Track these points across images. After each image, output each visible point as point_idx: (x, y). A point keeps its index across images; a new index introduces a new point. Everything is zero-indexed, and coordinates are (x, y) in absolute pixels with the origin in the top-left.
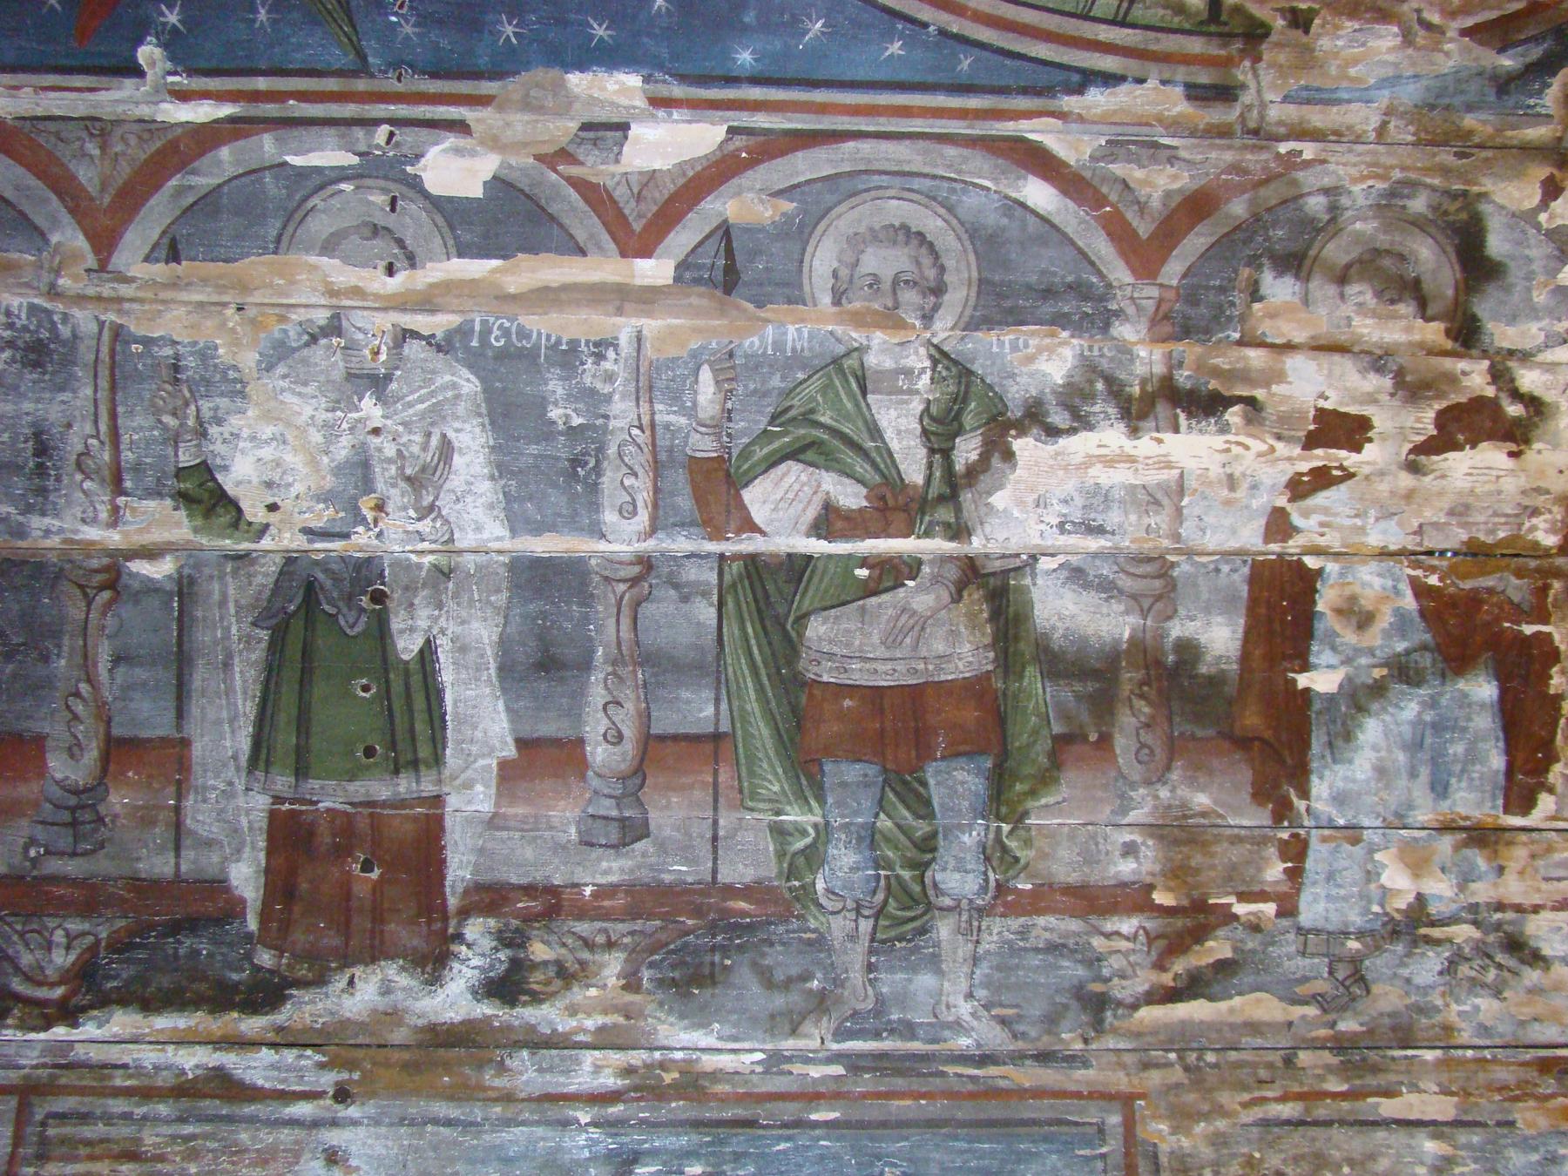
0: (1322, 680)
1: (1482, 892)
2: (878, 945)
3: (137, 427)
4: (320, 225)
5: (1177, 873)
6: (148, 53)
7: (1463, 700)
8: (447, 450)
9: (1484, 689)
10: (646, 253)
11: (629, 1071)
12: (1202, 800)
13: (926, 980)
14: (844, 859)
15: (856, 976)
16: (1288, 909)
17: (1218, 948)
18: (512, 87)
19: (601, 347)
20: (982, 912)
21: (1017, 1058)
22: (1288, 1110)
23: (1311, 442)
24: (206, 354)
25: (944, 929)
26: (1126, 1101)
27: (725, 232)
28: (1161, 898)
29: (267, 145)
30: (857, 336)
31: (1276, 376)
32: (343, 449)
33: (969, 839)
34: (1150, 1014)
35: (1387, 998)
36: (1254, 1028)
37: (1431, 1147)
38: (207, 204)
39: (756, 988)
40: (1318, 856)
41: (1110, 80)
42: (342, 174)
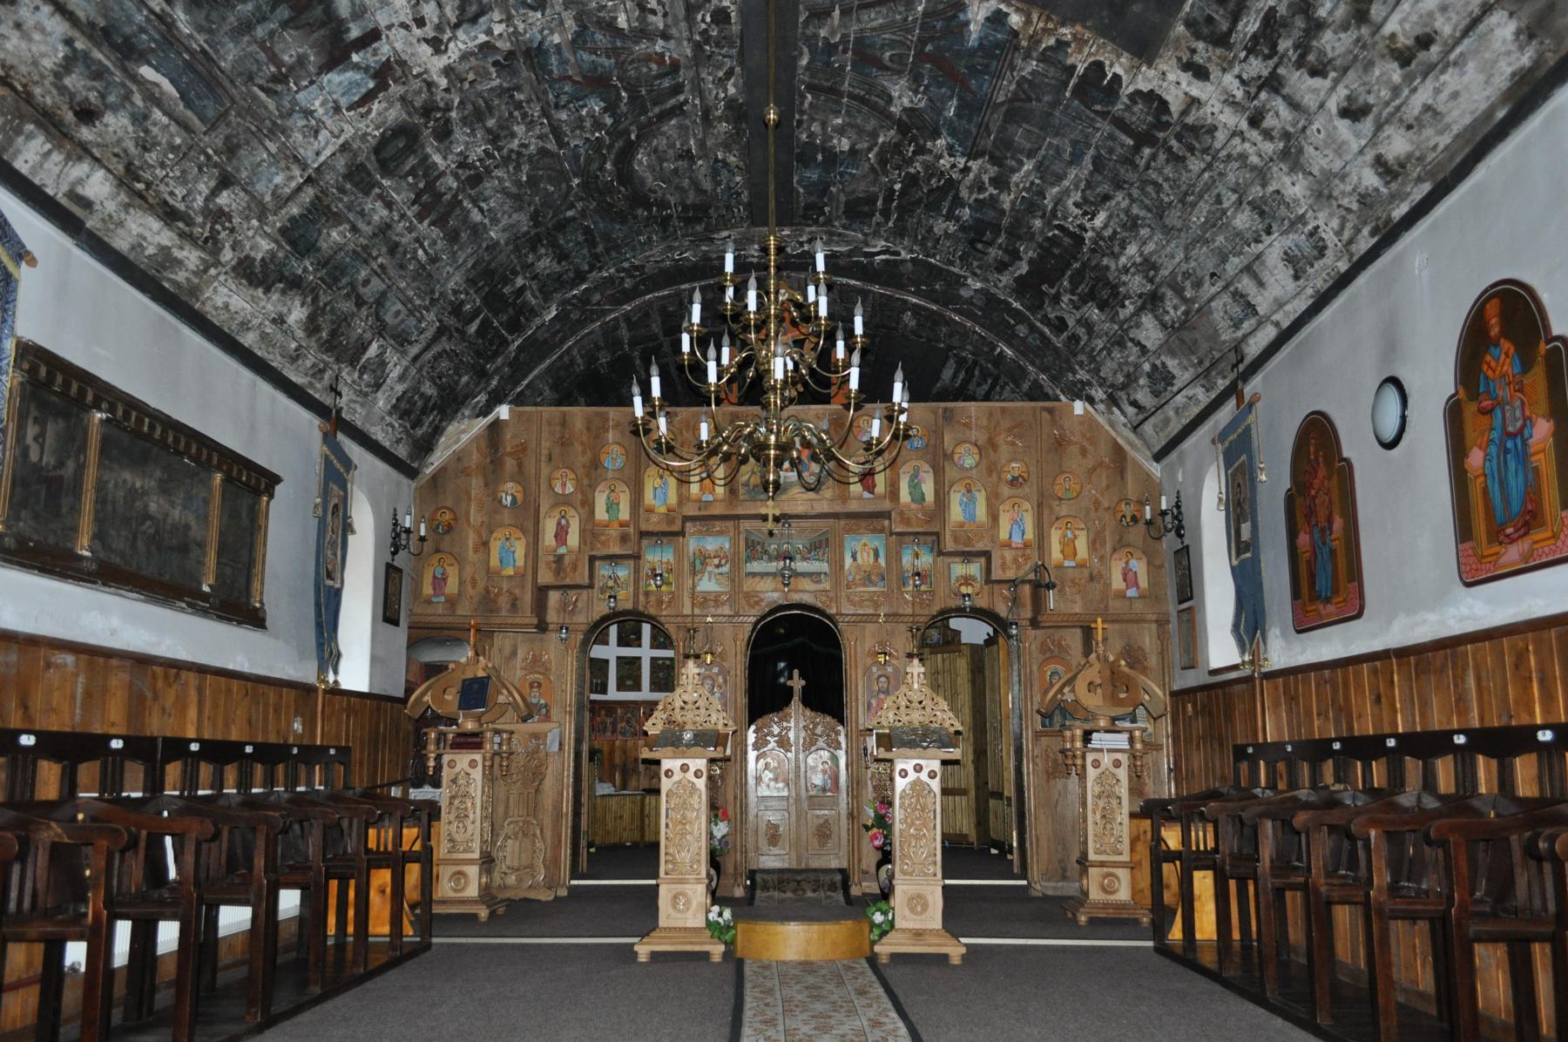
0: (355, 58)
1: (324, 118)
2: (233, 30)
5: (291, 68)
7: (366, 84)
9: (371, 85)
11: (163, 10)
12: (312, 58)
13: (231, 45)
15: (222, 32)
16: (296, 92)
17: (279, 88)
20: (256, 42)
21: (228, 77)
22: (253, 128)
23: (415, 20)
25: (246, 39)
26: (233, 101)
28: (284, 70)
30: (490, 418)
33: (272, 26)
34: (255, 89)
35: (289, 123)
36: (266, 108)
37: (265, 156)
39: (203, 16)
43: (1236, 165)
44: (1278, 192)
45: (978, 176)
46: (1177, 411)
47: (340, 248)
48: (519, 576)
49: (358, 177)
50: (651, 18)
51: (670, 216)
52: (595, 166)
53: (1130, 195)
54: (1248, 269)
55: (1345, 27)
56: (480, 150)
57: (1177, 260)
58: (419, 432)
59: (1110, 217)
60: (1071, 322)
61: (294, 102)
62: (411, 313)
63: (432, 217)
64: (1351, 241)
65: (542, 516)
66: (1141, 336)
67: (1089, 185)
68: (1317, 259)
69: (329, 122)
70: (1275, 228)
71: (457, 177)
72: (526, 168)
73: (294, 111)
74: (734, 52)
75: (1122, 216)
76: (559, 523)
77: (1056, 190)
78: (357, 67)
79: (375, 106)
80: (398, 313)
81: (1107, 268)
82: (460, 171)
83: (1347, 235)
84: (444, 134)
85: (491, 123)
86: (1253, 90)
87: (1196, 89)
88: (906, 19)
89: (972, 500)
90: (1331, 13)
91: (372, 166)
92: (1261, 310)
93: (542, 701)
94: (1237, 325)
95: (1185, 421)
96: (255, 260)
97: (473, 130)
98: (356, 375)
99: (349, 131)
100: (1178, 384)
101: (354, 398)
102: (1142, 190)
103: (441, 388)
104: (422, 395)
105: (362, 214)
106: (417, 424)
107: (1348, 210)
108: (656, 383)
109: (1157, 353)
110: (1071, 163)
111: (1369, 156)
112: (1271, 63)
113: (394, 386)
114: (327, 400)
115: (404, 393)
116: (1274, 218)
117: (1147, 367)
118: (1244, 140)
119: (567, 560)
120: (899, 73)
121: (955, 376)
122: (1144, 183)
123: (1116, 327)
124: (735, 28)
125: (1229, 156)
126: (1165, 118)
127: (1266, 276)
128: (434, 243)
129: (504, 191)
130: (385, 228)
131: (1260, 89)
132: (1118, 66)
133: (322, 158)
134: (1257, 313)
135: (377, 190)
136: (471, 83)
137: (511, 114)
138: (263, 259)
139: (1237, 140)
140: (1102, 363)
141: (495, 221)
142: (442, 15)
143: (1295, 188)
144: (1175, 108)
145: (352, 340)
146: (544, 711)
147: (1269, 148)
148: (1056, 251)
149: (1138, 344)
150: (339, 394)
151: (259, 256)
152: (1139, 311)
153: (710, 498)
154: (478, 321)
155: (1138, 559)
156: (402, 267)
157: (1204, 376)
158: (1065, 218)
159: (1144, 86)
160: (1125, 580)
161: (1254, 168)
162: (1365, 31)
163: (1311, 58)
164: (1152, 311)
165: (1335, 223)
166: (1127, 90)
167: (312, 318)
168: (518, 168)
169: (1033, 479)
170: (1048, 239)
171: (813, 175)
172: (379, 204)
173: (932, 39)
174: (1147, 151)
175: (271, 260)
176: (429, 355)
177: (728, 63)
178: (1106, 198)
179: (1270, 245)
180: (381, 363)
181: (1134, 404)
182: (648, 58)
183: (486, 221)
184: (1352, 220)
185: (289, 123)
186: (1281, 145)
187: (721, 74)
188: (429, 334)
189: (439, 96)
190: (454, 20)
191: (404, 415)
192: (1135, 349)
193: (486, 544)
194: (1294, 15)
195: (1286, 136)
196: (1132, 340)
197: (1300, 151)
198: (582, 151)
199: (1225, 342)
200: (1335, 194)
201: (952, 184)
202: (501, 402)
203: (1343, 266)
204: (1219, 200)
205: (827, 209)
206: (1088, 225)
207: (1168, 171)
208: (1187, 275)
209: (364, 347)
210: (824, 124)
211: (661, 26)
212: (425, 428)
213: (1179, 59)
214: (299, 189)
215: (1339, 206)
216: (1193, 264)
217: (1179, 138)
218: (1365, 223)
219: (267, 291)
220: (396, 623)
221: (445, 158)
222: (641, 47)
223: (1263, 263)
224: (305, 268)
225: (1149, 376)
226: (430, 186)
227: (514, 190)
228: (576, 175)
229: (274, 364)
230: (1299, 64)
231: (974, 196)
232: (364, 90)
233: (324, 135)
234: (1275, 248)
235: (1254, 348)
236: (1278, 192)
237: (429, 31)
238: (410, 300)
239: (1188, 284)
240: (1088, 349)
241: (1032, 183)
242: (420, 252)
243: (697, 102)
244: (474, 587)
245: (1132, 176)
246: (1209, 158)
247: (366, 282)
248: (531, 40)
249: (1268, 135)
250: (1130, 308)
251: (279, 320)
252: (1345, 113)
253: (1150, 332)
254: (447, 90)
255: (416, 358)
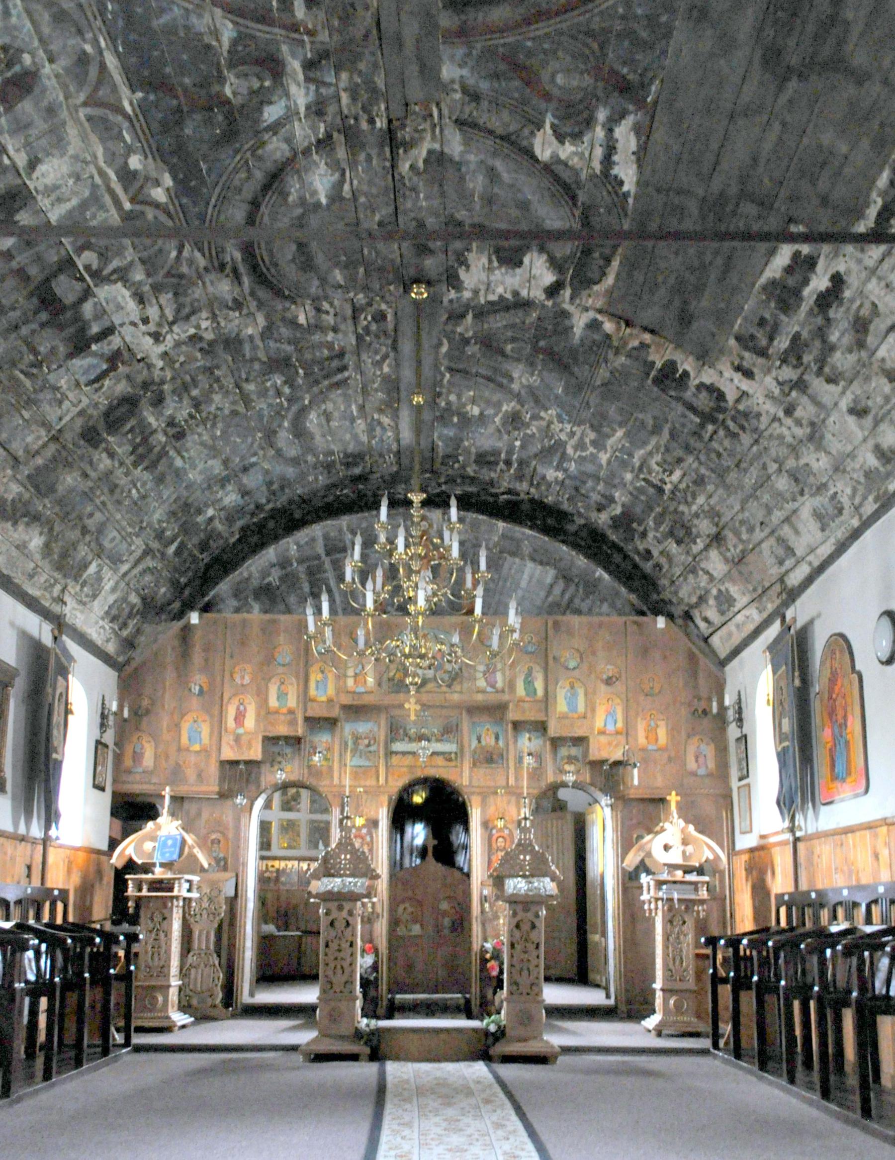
0: (94, 347)
3: (43, 142)
4: (110, 144)
6: (140, 95)
8: (69, 200)
9: (105, 367)
10: (131, 203)
14: (18, 313)
17: (35, 371)
18: (161, 164)
19: (108, 211)
24: (69, 143)
27: (143, 213)
29: (126, 125)
31: (151, 306)
32: (58, 183)
34: (17, 373)
37: (21, 422)
38: (104, 120)
40: (63, 369)
41: (204, 255)
42: (125, 142)
43: (776, 442)
44: (807, 465)
45: (582, 438)
46: (737, 626)
47: (71, 490)
48: (205, 751)
49: (91, 436)
50: (324, 316)
51: (334, 462)
52: (275, 424)
53: (698, 458)
54: (787, 520)
55: (850, 351)
56: (185, 413)
57: (736, 510)
58: (125, 633)
59: (684, 475)
60: (655, 553)
61: (45, 380)
62: (124, 538)
63: (145, 464)
64: (861, 505)
65: (225, 700)
66: (710, 567)
67: (667, 450)
68: (837, 516)
69: (71, 395)
70: (806, 490)
71: (166, 434)
72: (220, 425)
73: (45, 387)
74: (390, 342)
75: (693, 474)
76: (238, 709)
77: (642, 452)
78: (95, 354)
79: (107, 382)
80: (113, 539)
81: (683, 513)
82: (169, 429)
83: (857, 501)
84: (159, 401)
85: (195, 392)
86: (787, 390)
87: (745, 385)
88: (524, 323)
89: (575, 695)
90: (839, 339)
91: (101, 426)
92: (799, 552)
93: (221, 855)
94: (781, 563)
95: (744, 634)
96: (6, 500)
97: (181, 399)
98: (78, 588)
99: (85, 401)
100: (738, 606)
101: (76, 606)
102: (708, 455)
103: (144, 599)
104: (128, 603)
105: (91, 463)
106: (124, 625)
107: (859, 483)
108: (325, 606)
109: (722, 581)
110: (653, 433)
111: (871, 443)
112: (799, 371)
113: (107, 598)
114: (56, 609)
115: (115, 601)
116: (805, 483)
117: (714, 592)
118: (781, 424)
119: (244, 739)
120: (518, 360)
121: (563, 593)
122: (709, 450)
123: (690, 559)
124: (390, 326)
125: (771, 436)
126: (722, 404)
127: (801, 527)
128: (144, 484)
129: (203, 444)
130: (109, 473)
131: (791, 390)
132: (686, 364)
133: (64, 422)
134: (795, 555)
135: (104, 445)
136: (181, 364)
137: (211, 386)
138: (13, 500)
139: (776, 424)
140: (679, 587)
141: (194, 467)
142: (163, 315)
143: (819, 463)
144: (731, 397)
145: (77, 560)
146: (222, 863)
147: (799, 432)
148: (643, 498)
149: (707, 573)
150: (65, 603)
151: (10, 497)
152: (707, 548)
153: (362, 690)
154: (176, 544)
155: (707, 744)
156: (119, 502)
157: (757, 599)
158: (650, 473)
159: (707, 381)
160: (697, 761)
161: (789, 446)
162: (864, 354)
163: (827, 370)
164: (718, 548)
165: (849, 491)
166: (694, 382)
167: (47, 545)
168: (214, 425)
169: (623, 678)
170: (636, 488)
171: (450, 432)
172: (104, 455)
173: (544, 337)
174: (710, 428)
175: (20, 500)
176: (136, 571)
177: (384, 349)
178: (680, 460)
179: (803, 504)
180: (99, 578)
181: (706, 620)
182: (321, 345)
183: (187, 466)
184: (861, 490)
185: (41, 396)
186: (808, 430)
187: (378, 358)
188: (139, 553)
189: (157, 374)
190: (171, 319)
191: (113, 619)
192: (705, 577)
193: (177, 726)
194: (813, 339)
195: (812, 424)
196: (703, 570)
197: (822, 437)
198: (266, 413)
199: (772, 575)
200: (848, 469)
201: (561, 444)
202: (192, 608)
203: (855, 523)
204: (764, 467)
205: (461, 458)
206: (667, 480)
207: (727, 443)
208: (742, 522)
209: (86, 566)
210: (459, 396)
211: (332, 322)
212: (129, 630)
213: (733, 364)
214: (45, 445)
215: (851, 479)
216: (747, 514)
217: (734, 419)
218: (870, 492)
219: (15, 523)
220: (102, 789)
221: (157, 420)
222: (317, 337)
223: (798, 517)
224: (45, 506)
225: (716, 598)
226: (145, 440)
227: (210, 442)
228: (259, 431)
229: (16, 581)
230: (820, 372)
231: (578, 453)
232: (99, 371)
233: (66, 404)
234: (807, 506)
235: (795, 579)
236: (807, 465)
237: (152, 327)
238: (124, 529)
239: (744, 529)
240: (669, 576)
241: (623, 446)
242: (134, 491)
243: (359, 377)
244: (166, 760)
245: (699, 445)
246: (756, 436)
247: (91, 515)
248: (230, 332)
249: (799, 423)
250: (700, 544)
251: (21, 547)
252: (852, 411)
253: (715, 563)
254: (162, 369)
255: (125, 574)
